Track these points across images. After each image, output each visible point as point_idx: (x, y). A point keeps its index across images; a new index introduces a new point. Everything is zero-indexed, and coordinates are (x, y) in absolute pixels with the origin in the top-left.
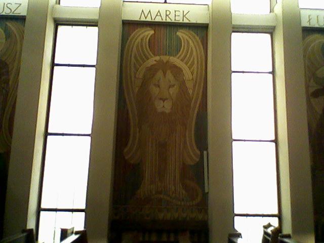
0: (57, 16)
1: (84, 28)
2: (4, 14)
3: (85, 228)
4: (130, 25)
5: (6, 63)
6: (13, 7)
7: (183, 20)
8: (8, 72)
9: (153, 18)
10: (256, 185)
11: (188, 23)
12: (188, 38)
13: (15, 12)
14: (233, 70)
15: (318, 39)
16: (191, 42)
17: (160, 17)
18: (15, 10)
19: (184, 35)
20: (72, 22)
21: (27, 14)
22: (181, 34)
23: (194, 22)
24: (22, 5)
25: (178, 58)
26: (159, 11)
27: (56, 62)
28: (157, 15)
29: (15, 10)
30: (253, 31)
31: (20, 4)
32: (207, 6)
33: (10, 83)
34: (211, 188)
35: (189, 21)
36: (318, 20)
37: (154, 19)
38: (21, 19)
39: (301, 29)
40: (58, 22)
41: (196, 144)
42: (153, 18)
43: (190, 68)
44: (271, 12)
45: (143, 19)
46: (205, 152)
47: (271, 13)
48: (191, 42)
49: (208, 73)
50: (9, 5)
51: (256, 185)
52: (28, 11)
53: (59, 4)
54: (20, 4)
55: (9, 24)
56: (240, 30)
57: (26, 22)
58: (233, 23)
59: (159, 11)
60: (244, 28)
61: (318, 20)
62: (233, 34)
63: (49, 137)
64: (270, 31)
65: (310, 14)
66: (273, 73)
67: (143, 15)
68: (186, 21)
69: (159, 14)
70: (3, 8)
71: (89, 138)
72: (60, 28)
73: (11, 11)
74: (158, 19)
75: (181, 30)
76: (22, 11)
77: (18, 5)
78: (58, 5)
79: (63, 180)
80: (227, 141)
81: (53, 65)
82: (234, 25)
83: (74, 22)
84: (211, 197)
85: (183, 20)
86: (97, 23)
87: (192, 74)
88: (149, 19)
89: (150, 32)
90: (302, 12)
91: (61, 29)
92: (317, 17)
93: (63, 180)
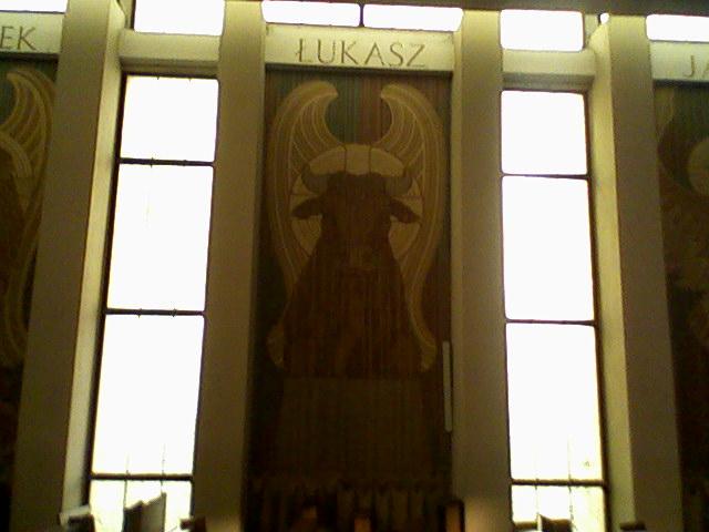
0: (125, 54)
1: (186, 80)
3: (192, 513)
4: (286, 76)
7: (19, 47)
9: (406, 61)
10: (555, 410)
11: (352, 68)
12: (30, 84)
13: (414, 63)
16: (36, 95)
19: (25, 82)
22: (392, 94)
23: (44, 51)
25: (4, 130)
26: (375, 46)
27: (124, 154)
30: (206, 73)
34: (459, 422)
35: (31, 47)
36: (693, 63)
37: (408, 65)
39: (651, 85)
43: (29, 150)
44: (584, 46)
46: (446, 346)
47: (586, 50)
48: (36, 95)
49: (453, 172)
51: (555, 410)
53: (132, 27)
57: (60, 68)
58: (504, 70)
59: (375, 46)
61: (693, 63)
62: (506, 95)
63: (109, 319)
64: (583, 86)
65: (302, 36)
68: (25, 49)
72: (133, 82)
74: (374, 63)
75: (19, 70)
78: (130, 31)
79: (144, 405)
80: (492, 324)
81: (118, 160)
82: (509, 74)
84: (460, 442)
85: (19, 47)
87: (33, 164)
89: (326, 92)
90: (654, 47)
91: (134, 83)
92: (301, 42)
93: (144, 405)
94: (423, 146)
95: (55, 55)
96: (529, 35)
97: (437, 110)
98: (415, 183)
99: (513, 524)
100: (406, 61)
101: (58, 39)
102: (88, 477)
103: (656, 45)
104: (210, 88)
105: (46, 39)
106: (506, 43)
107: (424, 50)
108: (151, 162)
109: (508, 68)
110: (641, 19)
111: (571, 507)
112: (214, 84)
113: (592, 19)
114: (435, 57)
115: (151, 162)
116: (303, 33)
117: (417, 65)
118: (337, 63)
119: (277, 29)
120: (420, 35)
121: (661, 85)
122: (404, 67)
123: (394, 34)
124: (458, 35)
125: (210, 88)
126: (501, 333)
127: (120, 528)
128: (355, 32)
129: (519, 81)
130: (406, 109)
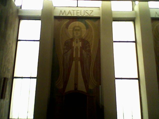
2: (84, 16)
5: (88, 41)
6: (89, 12)
8: (89, 46)
9: (67, 14)
14: (114, 40)
15: (158, 24)
20: (121, 19)
26: (65, 11)
31: (93, 11)
32: (98, 8)
33: (91, 51)
38: (97, 19)
40: (21, 18)
42: (72, 14)
45: (61, 15)
55: (88, 22)
59: (65, 11)
64: (133, 20)
66: (135, 42)
71: (36, 79)
74: (69, 15)
80: (112, 79)
83: (123, 19)
88: (64, 15)
96: (118, 8)
97: (153, 31)
99: (37, 77)
103: (150, 9)
104: (39, 22)
106: (113, 10)
108: (34, 41)
109: (114, 16)
110: (147, 2)
111: (132, 116)
113: (134, 2)
114: (96, 13)
118: (75, 15)
119: (56, 8)
120: (93, 8)
123: (86, 8)
124: (101, 8)
125: (39, 22)
127: (32, 117)
128: (75, 8)
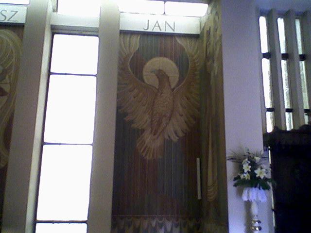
0: (53, 23)
1: (83, 36)
7: (165, 30)
9: (7, 19)
13: (11, 19)
17: (158, 27)
18: (10, 18)
21: (26, 22)
24: (18, 13)
26: (157, 22)
28: (155, 26)
29: (10, 18)
31: (17, 12)
37: (8, 20)
41: (279, 89)
50: (3, 12)
52: (26, 18)
54: (17, 12)
56: (72, 32)
57: (25, 29)
59: (157, 22)
60: (66, 30)
63: (45, 146)
67: (167, 26)
69: (157, 25)
70: (147, 25)
72: (56, 36)
73: (6, 17)
74: (157, 30)
76: (20, 18)
77: (14, 13)
78: (55, 13)
79: (65, 181)
86: (98, 32)
92: (148, 21)
93: (65, 181)
94: (14, 60)
95: (23, 24)
98: (7, 77)
100: (7, 19)
101: (25, 19)
102: (35, 222)
104: (95, 40)
105: (20, 17)
107: (17, 14)
108: (66, 74)
112: (97, 39)
115: (66, 74)
116: (15, 8)
117: (12, 21)
121: (124, 33)
122: (6, 21)
125: (95, 40)
126: (92, 194)
129: (57, 29)
130: (7, 41)
